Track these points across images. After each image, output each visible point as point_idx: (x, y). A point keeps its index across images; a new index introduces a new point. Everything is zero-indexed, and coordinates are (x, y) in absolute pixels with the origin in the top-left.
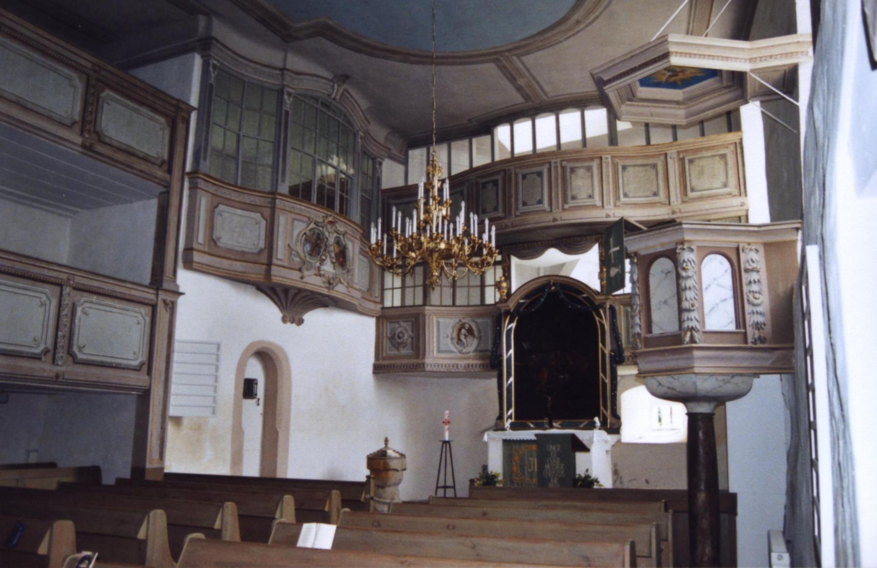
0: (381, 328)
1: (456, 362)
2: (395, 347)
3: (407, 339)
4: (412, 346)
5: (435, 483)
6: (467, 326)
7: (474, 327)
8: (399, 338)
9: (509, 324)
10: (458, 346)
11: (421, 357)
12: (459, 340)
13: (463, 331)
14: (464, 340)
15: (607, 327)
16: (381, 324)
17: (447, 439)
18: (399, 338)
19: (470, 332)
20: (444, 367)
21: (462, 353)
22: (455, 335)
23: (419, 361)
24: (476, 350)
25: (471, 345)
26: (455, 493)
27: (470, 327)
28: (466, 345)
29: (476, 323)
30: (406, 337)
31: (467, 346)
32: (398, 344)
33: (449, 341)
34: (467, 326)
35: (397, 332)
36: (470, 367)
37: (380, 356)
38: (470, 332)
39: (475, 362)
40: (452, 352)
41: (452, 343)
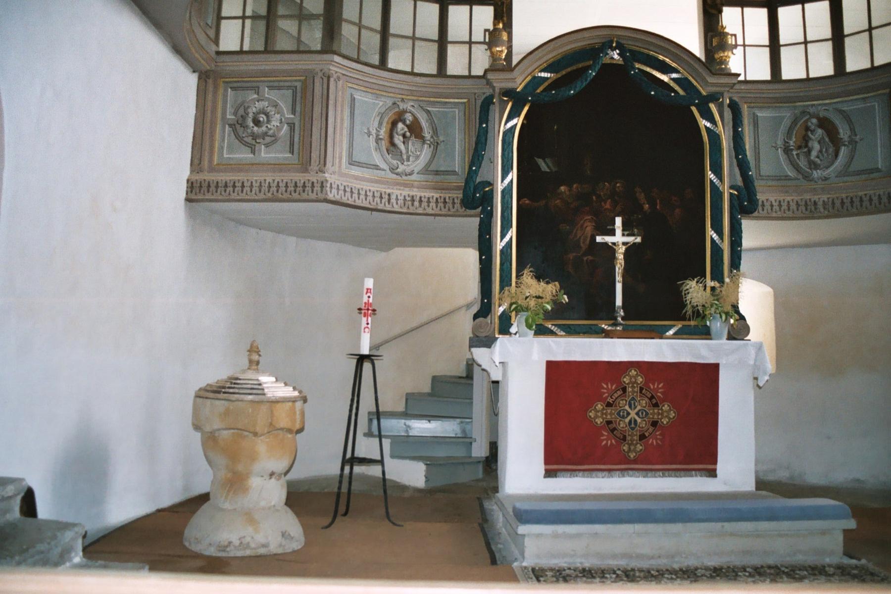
0: (209, 104)
1: (388, 191)
2: (246, 144)
3: (279, 129)
4: (292, 144)
5: (341, 454)
6: (409, 118)
7: (424, 124)
8: (257, 123)
9: (509, 119)
10: (389, 157)
11: (314, 166)
12: (392, 144)
13: (400, 125)
14: (402, 147)
15: (726, 143)
16: (211, 88)
17: (365, 351)
18: (257, 123)
19: (415, 129)
20: (363, 197)
21: (397, 174)
22: (383, 133)
23: (313, 177)
24: (426, 170)
25: (418, 157)
26: (384, 473)
27: (416, 120)
28: (405, 157)
29: (428, 112)
30: (275, 123)
31: (408, 160)
32: (254, 137)
33: (372, 143)
34: (409, 118)
35: (252, 110)
36: (416, 204)
37: (206, 163)
38: (415, 129)
39: (428, 194)
40: (377, 167)
41: (378, 149)
